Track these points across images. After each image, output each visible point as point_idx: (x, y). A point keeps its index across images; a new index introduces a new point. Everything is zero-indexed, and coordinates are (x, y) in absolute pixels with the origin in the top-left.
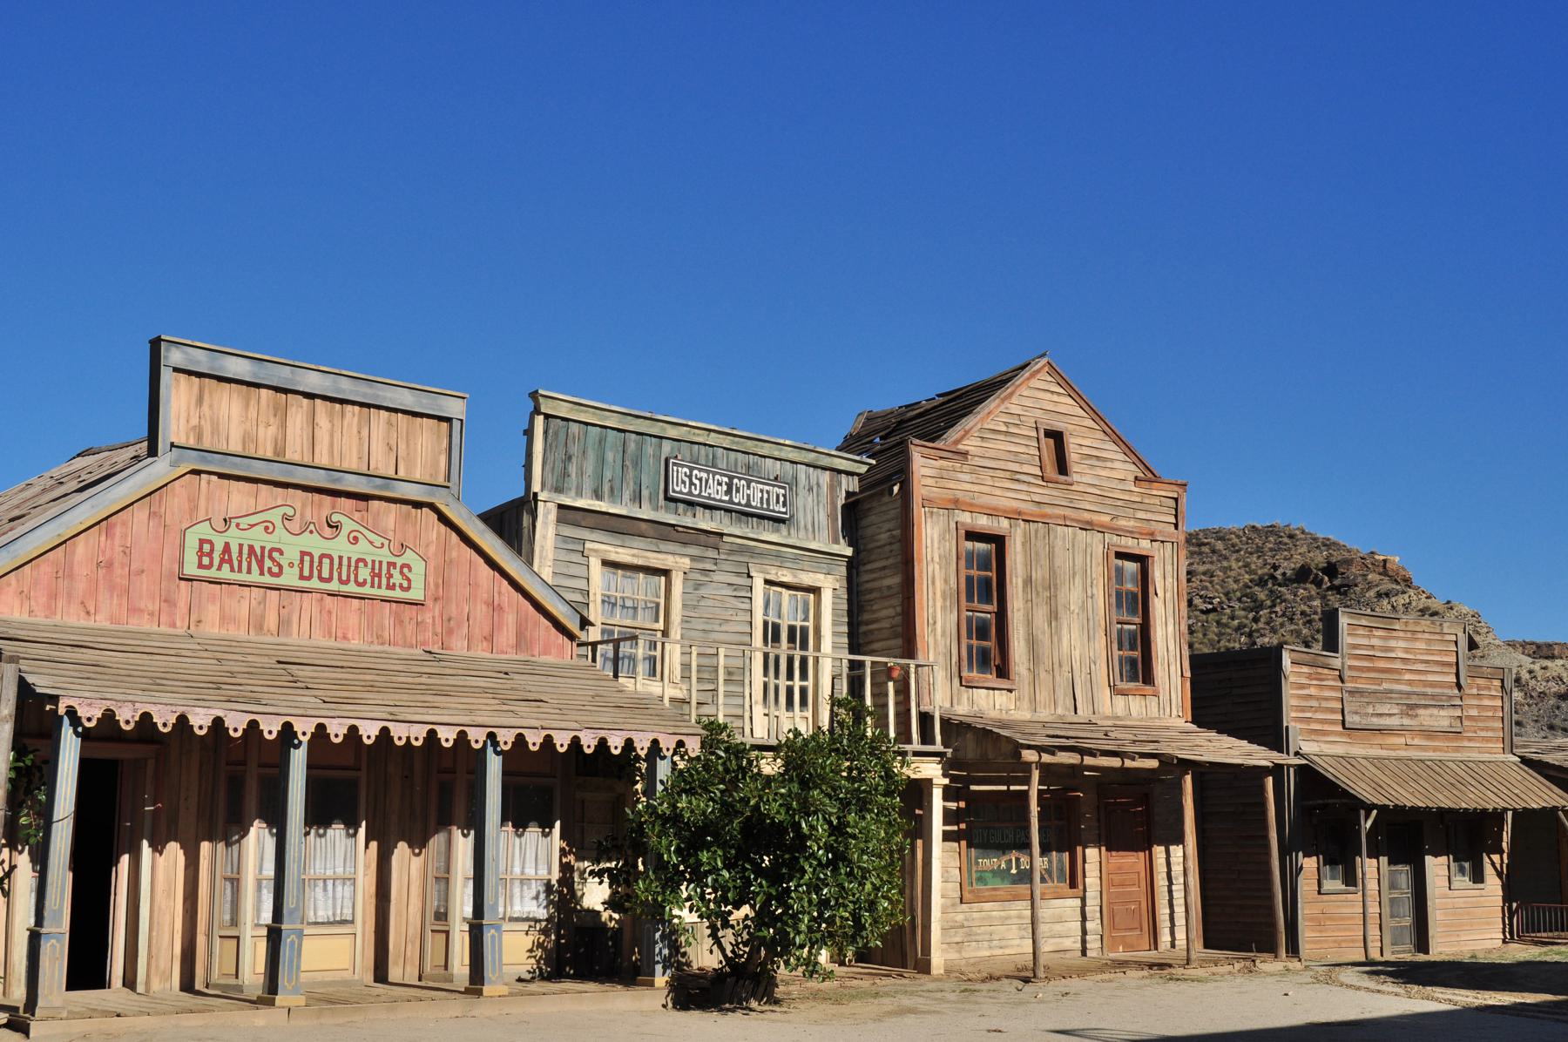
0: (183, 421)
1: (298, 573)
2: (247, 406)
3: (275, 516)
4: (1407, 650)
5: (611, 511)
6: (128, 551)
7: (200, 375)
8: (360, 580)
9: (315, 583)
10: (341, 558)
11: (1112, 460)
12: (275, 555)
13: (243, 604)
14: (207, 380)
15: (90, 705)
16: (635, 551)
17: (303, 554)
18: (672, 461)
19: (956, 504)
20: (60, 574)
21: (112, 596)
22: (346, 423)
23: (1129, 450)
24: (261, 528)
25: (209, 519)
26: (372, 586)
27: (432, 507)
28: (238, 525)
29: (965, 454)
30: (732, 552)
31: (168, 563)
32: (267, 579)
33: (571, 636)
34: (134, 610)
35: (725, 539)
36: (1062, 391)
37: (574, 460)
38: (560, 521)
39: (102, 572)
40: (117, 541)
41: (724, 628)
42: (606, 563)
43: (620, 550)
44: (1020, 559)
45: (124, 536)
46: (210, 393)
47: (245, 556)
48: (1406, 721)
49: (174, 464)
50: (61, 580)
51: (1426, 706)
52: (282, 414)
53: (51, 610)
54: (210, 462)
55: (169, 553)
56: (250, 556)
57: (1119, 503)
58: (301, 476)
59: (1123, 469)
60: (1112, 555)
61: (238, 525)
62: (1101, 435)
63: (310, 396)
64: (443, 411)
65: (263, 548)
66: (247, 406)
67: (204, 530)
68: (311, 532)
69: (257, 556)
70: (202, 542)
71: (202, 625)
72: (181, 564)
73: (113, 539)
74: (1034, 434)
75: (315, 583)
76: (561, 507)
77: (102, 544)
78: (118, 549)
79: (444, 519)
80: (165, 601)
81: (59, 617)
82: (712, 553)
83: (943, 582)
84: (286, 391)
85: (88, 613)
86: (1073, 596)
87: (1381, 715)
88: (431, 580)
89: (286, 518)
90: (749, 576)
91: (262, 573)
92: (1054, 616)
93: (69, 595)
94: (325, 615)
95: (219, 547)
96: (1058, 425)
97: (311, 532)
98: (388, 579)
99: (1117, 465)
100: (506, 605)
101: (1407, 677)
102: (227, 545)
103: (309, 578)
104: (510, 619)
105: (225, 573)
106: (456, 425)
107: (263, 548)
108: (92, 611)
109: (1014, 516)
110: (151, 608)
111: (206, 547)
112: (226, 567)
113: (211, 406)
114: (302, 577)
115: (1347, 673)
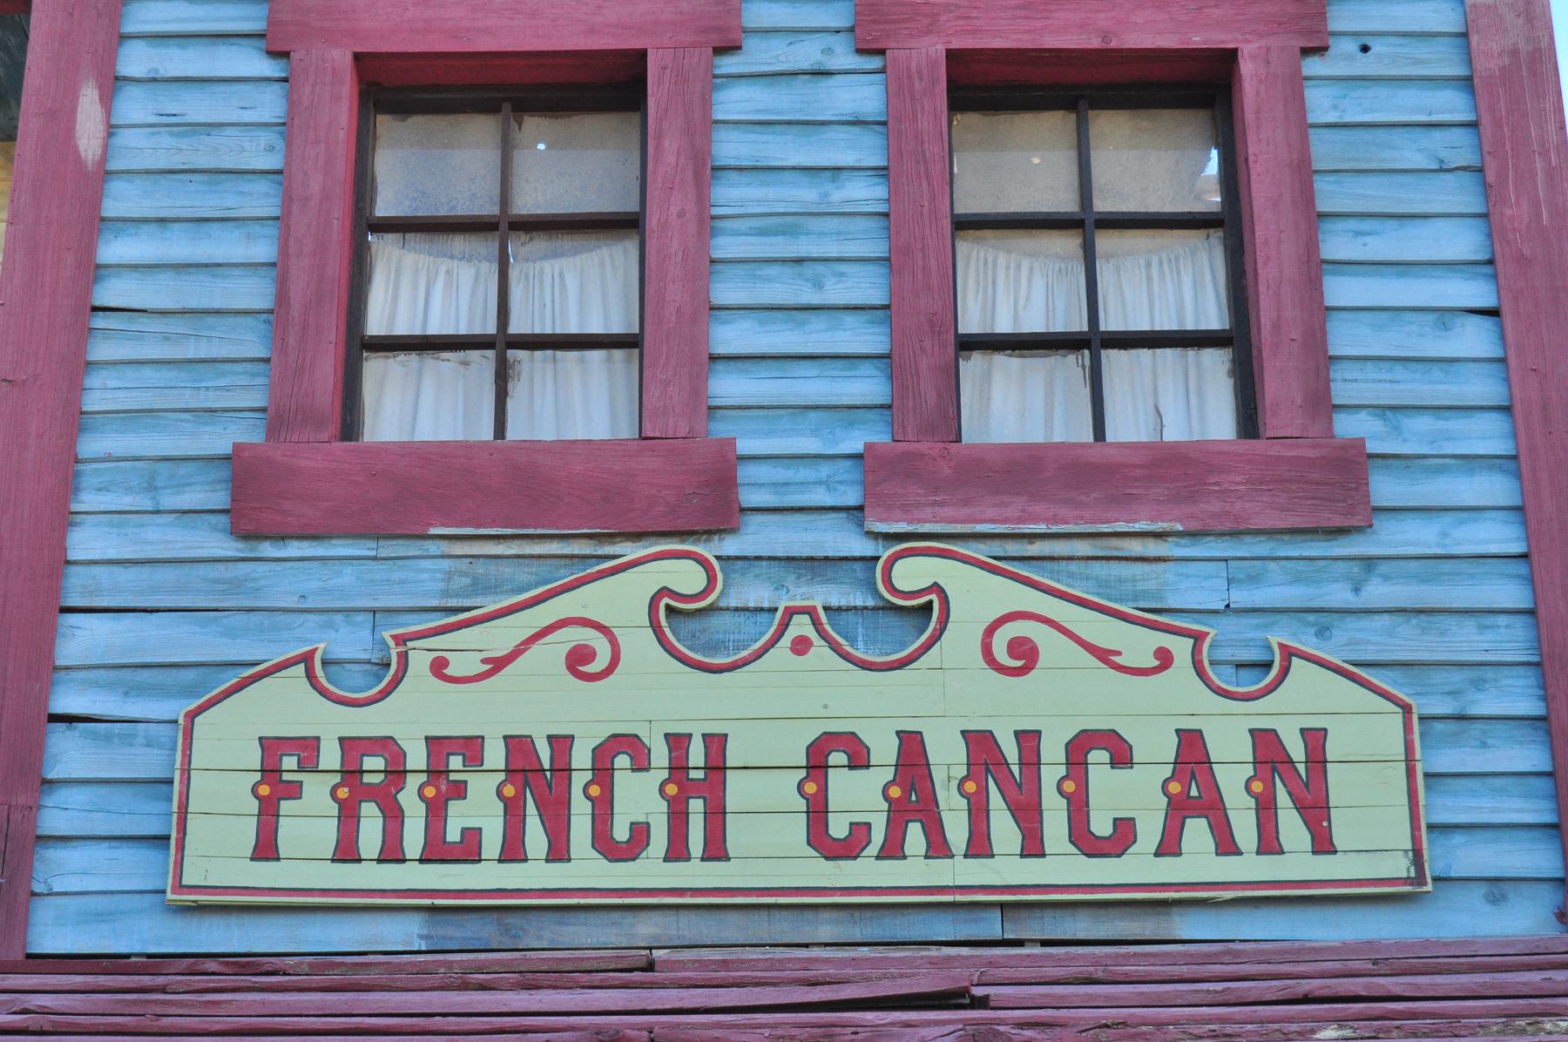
8: (838, 828)
26: (677, 851)
28: (439, 668)
44: (757, 414)
61: (439, 668)
68: (800, 646)
70: (272, 747)
83: (100, 493)
98: (436, 812)
112: (1197, 831)
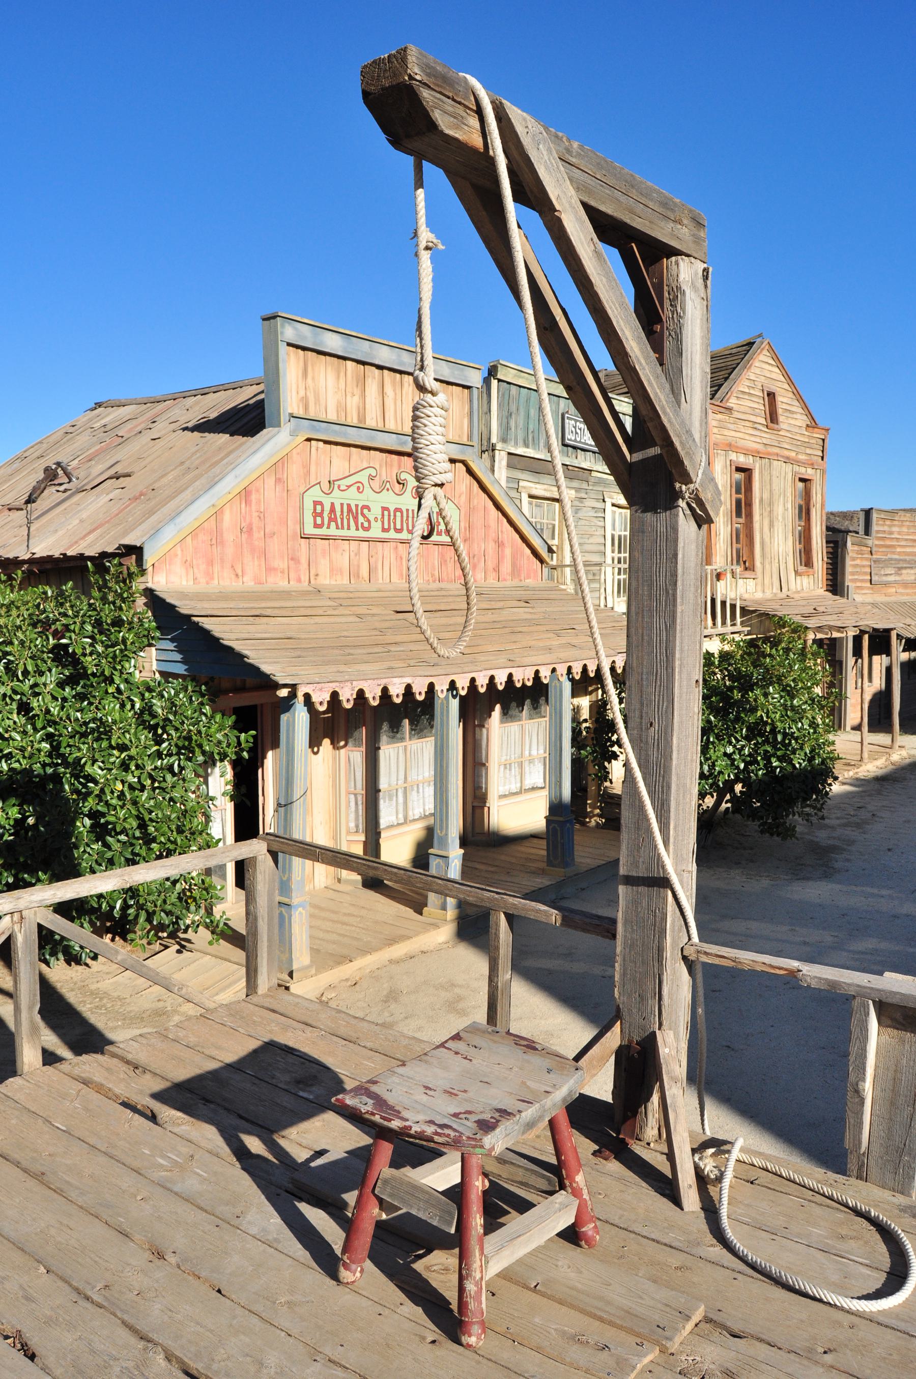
0: (294, 393)
1: (381, 526)
2: (338, 378)
3: (363, 477)
4: (899, 533)
5: (537, 456)
6: (262, 515)
7: (304, 349)
9: (392, 534)
10: (407, 510)
11: (796, 413)
12: (365, 511)
13: (343, 555)
14: (310, 353)
15: (321, 690)
16: (546, 486)
17: (384, 509)
18: (567, 415)
19: (730, 447)
20: (214, 542)
21: (253, 558)
22: (404, 392)
23: (805, 407)
24: (354, 488)
25: (319, 483)
27: (463, 462)
28: (339, 487)
29: (730, 409)
30: (595, 484)
31: (293, 527)
32: (361, 533)
33: (542, 561)
34: (270, 570)
35: (594, 474)
36: (773, 363)
37: (513, 416)
38: (509, 466)
39: (244, 536)
40: (254, 508)
41: (591, 541)
42: (531, 496)
43: (538, 486)
45: (258, 502)
46: (312, 366)
47: (345, 514)
48: (897, 578)
49: (293, 434)
50: (214, 547)
51: (906, 568)
52: (362, 382)
53: (210, 576)
54: (318, 431)
55: (292, 516)
56: (348, 515)
57: (799, 443)
58: (353, 436)
59: (801, 420)
60: (797, 480)
61: (339, 487)
62: (791, 395)
63: (380, 367)
64: (468, 381)
65: (357, 506)
66: (338, 378)
67: (315, 494)
68: (388, 490)
69: (355, 513)
70: (316, 503)
71: (319, 578)
72: (302, 523)
73: (250, 506)
74: (761, 394)
75: (392, 534)
76: (509, 454)
77: (243, 511)
78: (255, 514)
79: (470, 471)
80: (292, 559)
81: (216, 582)
82: (585, 485)
84: (364, 363)
85: (237, 575)
86: (779, 510)
87: (887, 575)
88: (462, 525)
89: (371, 478)
90: (604, 501)
91: (357, 529)
92: (771, 525)
93: (222, 560)
94: (399, 559)
95: (327, 508)
96: (773, 389)
97: (388, 490)
99: (798, 416)
100: (506, 542)
101: (898, 550)
102: (333, 504)
103: (388, 530)
104: (508, 552)
105: (333, 531)
106: (475, 391)
107: (357, 506)
108: (240, 574)
109: (756, 454)
110: (281, 567)
111: (319, 508)
112: (333, 524)
113: (313, 378)
114: (384, 530)
115: (874, 549)
